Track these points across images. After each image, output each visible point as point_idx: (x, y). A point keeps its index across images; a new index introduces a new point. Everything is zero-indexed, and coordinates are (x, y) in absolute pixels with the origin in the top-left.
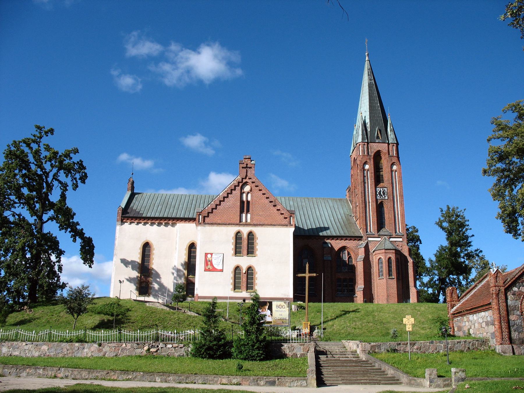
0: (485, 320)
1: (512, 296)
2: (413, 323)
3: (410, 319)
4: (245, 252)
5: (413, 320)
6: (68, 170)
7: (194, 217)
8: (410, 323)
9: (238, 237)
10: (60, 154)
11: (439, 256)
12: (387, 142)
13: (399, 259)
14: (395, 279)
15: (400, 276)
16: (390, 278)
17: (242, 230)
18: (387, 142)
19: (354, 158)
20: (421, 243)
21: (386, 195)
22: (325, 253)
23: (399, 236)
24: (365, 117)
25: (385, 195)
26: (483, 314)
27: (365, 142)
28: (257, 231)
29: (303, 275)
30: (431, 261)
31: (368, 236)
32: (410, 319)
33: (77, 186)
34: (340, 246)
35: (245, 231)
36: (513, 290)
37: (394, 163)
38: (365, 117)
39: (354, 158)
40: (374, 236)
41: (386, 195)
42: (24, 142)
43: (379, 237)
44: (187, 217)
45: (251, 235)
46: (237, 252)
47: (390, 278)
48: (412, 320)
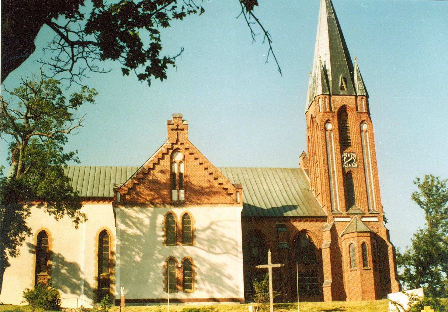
13: (376, 244)
14: (372, 271)
16: (365, 269)
18: (355, 94)
21: (355, 162)
23: (374, 215)
25: (354, 163)
27: (327, 95)
31: (334, 215)
37: (364, 120)
40: (341, 215)
41: (355, 162)
43: (349, 217)
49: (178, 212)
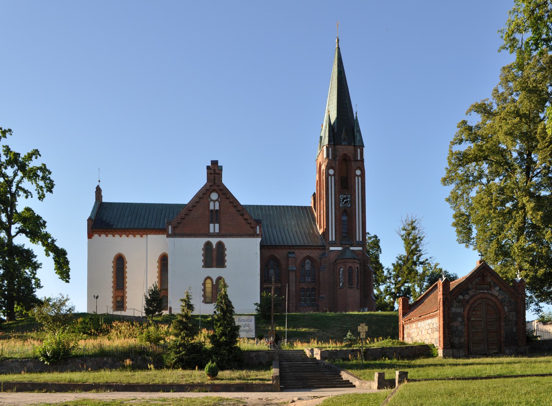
0: (431, 327)
1: (457, 304)
2: (367, 330)
3: (364, 327)
4: (214, 263)
5: (366, 327)
6: (32, 175)
7: (164, 228)
8: (364, 331)
9: (208, 245)
10: (22, 156)
11: (397, 267)
12: (353, 144)
15: (359, 285)
16: (350, 288)
17: (211, 241)
19: (320, 162)
20: (381, 253)
22: (289, 263)
24: (356, 113)
26: (429, 321)
28: (228, 242)
29: (291, 329)
30: (388, 270)
32: (364, 327)
33: (44, 196)
34: (305, 255)
35: (214, 241)
36: (459, 298)
38: (356, 113)
39: (320, 162)
42: (453, 143)
44: (158, 228)
45: (221, 245)
46: (208, 264)
47: (350, 288)
48: (366, 328)
49: (214, 241)
